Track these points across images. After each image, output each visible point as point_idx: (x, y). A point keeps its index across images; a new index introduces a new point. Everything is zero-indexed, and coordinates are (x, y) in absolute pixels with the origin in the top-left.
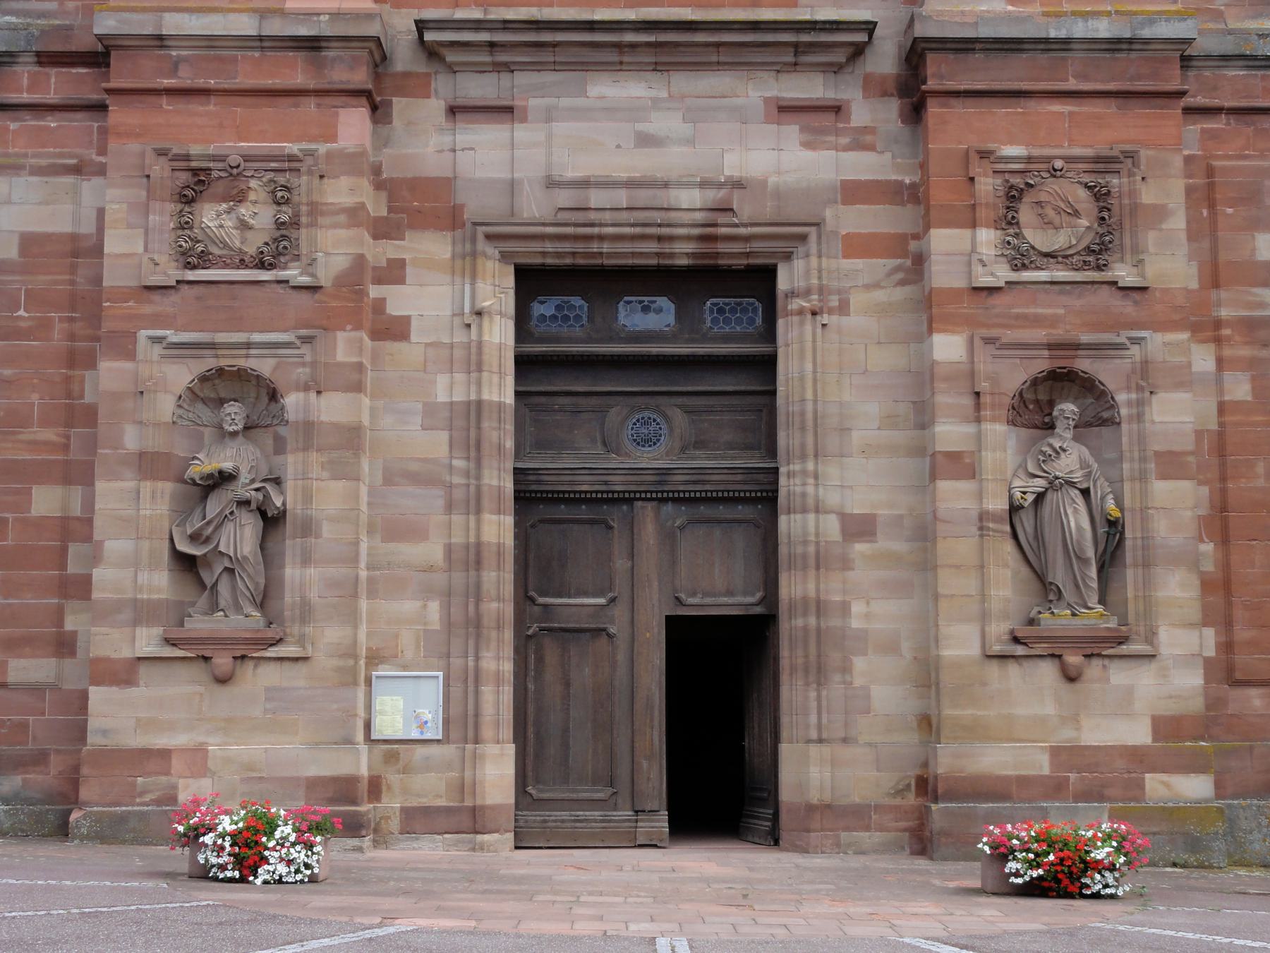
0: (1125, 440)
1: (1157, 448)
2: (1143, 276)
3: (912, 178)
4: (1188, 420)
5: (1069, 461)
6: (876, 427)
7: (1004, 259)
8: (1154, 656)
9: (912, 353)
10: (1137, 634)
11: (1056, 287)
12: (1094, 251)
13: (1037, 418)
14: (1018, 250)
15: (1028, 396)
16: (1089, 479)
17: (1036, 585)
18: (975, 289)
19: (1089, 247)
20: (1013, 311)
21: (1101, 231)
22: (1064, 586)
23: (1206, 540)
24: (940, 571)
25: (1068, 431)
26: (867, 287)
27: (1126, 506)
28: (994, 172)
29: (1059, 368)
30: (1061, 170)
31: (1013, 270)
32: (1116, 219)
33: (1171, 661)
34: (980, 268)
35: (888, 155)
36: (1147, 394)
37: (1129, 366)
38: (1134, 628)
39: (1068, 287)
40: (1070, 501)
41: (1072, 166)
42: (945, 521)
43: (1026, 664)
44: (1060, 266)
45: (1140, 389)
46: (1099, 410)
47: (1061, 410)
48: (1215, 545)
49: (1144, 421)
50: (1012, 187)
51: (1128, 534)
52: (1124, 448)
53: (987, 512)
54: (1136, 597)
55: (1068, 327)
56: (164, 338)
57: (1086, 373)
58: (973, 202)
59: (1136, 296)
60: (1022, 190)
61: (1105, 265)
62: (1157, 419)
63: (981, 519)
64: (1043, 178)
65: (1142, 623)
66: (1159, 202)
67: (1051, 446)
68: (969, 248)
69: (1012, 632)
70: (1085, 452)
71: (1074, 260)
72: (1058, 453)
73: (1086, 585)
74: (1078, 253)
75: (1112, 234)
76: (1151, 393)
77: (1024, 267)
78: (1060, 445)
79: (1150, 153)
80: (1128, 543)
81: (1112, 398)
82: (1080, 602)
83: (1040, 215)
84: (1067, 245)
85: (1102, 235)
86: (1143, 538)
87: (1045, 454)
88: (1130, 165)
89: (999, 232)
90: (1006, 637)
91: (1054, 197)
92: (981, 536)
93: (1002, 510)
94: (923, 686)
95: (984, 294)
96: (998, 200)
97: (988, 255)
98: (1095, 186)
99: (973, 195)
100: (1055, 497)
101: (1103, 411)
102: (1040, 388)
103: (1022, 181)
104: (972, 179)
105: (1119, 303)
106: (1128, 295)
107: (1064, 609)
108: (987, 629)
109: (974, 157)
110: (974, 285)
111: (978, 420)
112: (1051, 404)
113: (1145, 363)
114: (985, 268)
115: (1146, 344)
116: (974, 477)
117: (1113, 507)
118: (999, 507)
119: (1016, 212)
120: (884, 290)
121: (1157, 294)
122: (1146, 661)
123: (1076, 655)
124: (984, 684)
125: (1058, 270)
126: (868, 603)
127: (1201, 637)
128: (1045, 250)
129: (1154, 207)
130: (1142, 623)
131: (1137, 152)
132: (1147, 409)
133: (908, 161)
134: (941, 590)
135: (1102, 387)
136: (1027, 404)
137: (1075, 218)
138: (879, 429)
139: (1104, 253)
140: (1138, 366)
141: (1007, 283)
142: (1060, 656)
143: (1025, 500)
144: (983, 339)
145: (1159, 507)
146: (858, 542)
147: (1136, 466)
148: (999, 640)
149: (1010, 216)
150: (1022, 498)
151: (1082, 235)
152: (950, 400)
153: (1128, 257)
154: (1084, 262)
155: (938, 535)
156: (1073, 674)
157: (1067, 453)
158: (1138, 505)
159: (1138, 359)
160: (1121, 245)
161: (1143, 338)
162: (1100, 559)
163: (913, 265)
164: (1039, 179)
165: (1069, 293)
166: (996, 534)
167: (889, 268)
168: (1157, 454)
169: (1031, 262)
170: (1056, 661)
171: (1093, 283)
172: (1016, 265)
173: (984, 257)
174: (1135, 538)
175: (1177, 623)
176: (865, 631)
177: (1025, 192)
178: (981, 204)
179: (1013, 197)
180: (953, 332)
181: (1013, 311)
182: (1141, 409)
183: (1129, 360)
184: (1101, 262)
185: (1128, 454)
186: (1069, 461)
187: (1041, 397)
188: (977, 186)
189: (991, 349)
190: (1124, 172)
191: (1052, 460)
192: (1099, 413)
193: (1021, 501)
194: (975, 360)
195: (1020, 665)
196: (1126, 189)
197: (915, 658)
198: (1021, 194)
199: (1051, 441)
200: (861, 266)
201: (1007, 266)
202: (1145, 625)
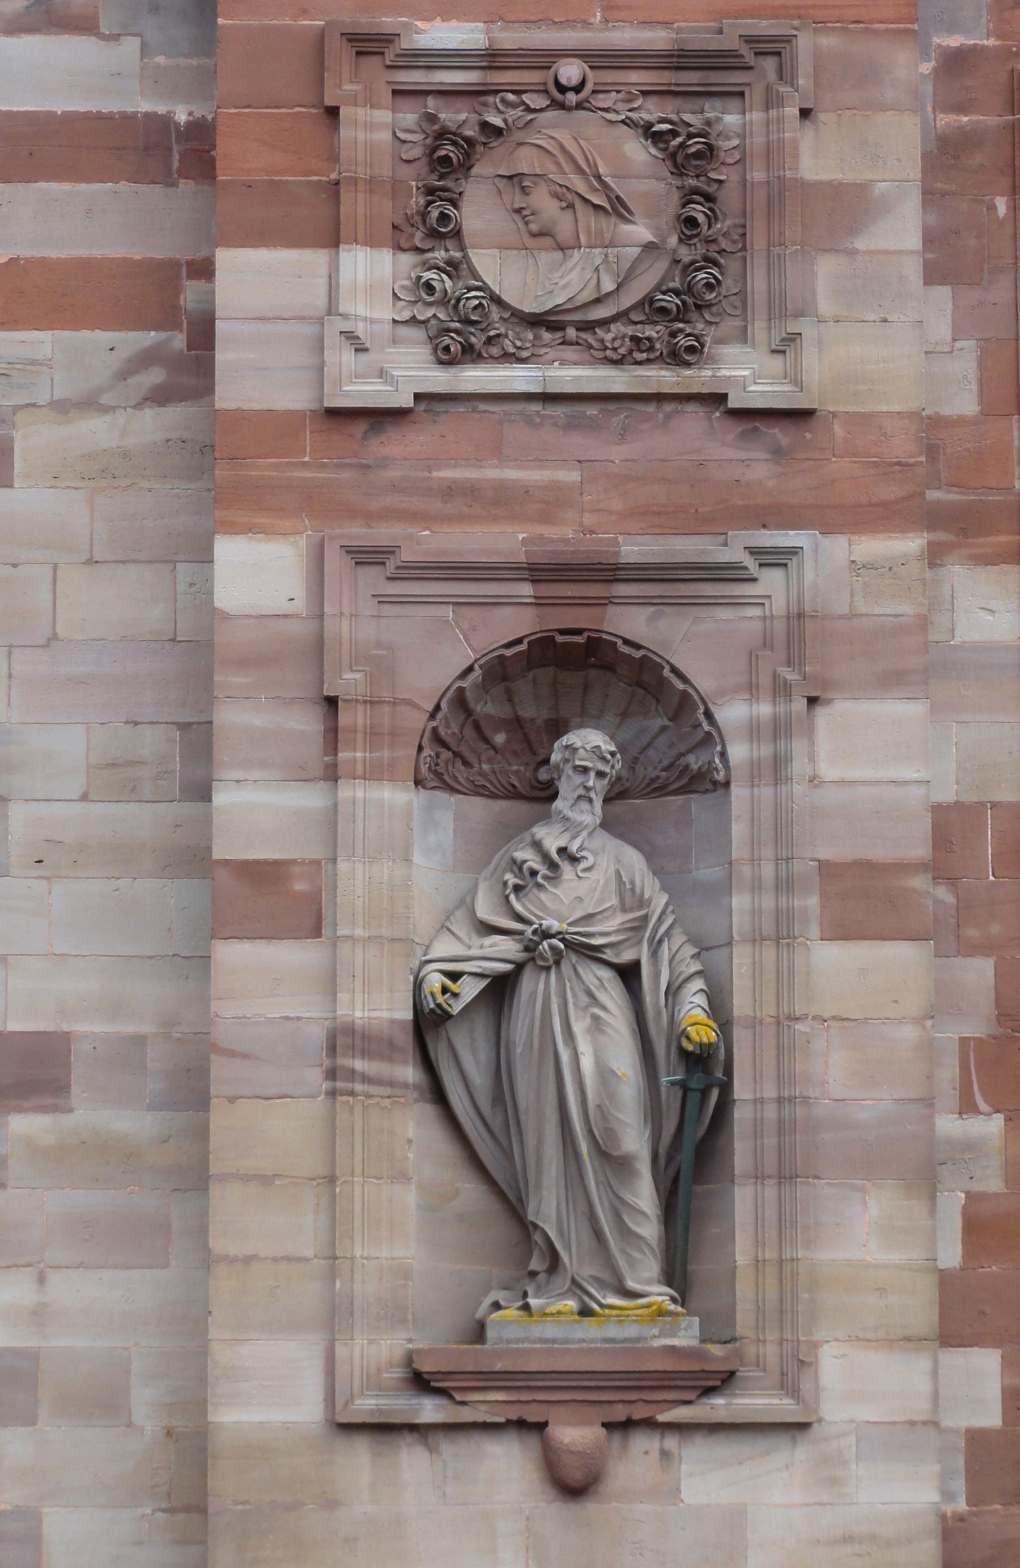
0: (738, 830)
1: (827, 853)
2: (798, 383)
3: (192, 107)
4: (916, 776)
5: (582, 889)
6: (75, 796)
7: (418, 334)
8: (803, 1427)
9: (181, 588)
10: (759, 1363)
11: (559, 411)
12: (664, 311)
13: (517, 771)
14: (456, 307)
15: (485, 708)
16: (640, 942)
17: (502, 1230)
18: (337, 415)
19: (652, 301)
20: (435, 474)
21: (685, 254)
22: (560, 1232)
23: (983, 1106)
24: (215, 1190)
25: (584, 805)
26: (62, 407)
27: (736, 1012)
28: (395, 92)
29: (563, 632)
30: (578, 89)
31: (441, 362)
32: (728, 222)
33: (852, 1439)
34: (348, 356)
35: (131, 46)
36: (799, 705)
37: (758, 625)
38: (751, 1351)
39: (592, 410)
40: (584, 999)
41: (610, 76)
42: (231, 1053)
43: (449, 1448)
44: (570, 353)
45: (781, 690)
46: (683, 747)
47: (567, 747)
48: (1008, 1119)
49: (789, 780)
50: (443, 134)
51: (741, 1090)
52: (735, 855)
53: (350, 1030)
54: (758, 1264)
55: (589, 520)
56: (390, 551)
57: (637, 646)
58: (333, 176)
59: (778, 434)
60: (469, 141)
61: (691, 350)
62: (828, 771)
63: (332, 1049)
64: (529, 110)
65: (772, 1336)
66: (849, 177)
67: (537, 845)
68: (322, 302)
69: (409, 1359)
70: (634, 860)
71: (609, 337)
72: (553, 866)
73: (625, 1232)
74: (621, 316)
75: (715, 263)
76: (812, 701)
77: (470, 354)
78: (562, 843)
79: (828, 42)
80: (741, 1115)
81: (708, 715)
82: (606, 1276)
83: (518, 211)
84: (588, 295)
85: (690, 268)
86: (780, 1100)
87: (520, 869)
88: (772, 76)
89: (407, 259)
90: (398, 1373)
91: (558, 164)
92: (333, 1094)
93: (393, 1021)
94: (189, 1509)
95: (360, 427)
96: (406, 172)
97: (372, 321)
98: (674, 133)
99: (333, 157)
100: (541, 986)
101: (690, 751)
102: (522, 687)
103: (474, 117)
104: (333, 112)
105: (731, 454)
106: (756, 429)
107: (562, 1296)
108: (341, 1351)
109: (340, 54)
110: (327, 404)
111: (332, 775)
112: (558, 728)
113: (798, 617)
114: (363, 357)
115: (800, 566)
116: (317, 932)
117: (700, 1015)
118: (385, 1014)
119: (455, 204)
120: (108, 418)
121: (838, 429)
122: (781, 1441)
123: (587, 1423)
124: (332, 1504)
125: (563, 362)
126: (41, 1280)
127: (935, 1374)
128: (529, 307)
129: (836, 191)
130: (772, 1336)
131: (788, 39)
132: (798, 746)
133: (182, 61)
134: (218, 1244)
135: (681, 686)
136: (488, 732)
137: (613, 219)
138: (84, 798)
139: (694, 315)
140: (779, 627)
141: (418, 397)
142: (541, 1427)
143: (455, 995)
144: (350, 551)
145: (827, 1015)
146: (20, 1110)
147: (768, 902)
148: (373, 1384)
149: (435, 214)
150: (445, 990)
151: (632, 269)
152: (259, 721)
153: (758, 328)
154: (635, 339)
155: (213, 1090)
156: (575, 1475)
157: (583, 865)
158: (769, 1010)
159: (778, 606)
160: (742, 294)
161: (794, 551)
162: (670, 1158)
163: (190, 348)
164: (518, 112)
165: (593, 426)
166: (374, 1090)
167: (124, 353)
168: (827, 869)
169: (490, 341)
170: (533, 1441)
171: (659, 398)
172: (447, 349)
173: (361, 325)
174: (759, 1102)
175: (870, 1335)
176: (33, 1356)
177: (480, 148)
178: (355, 181)
179: (446, 160)
180: (269, 532)
181: (435, 474)
182: (782, 744)
183: (756, 612)
184: (683, 341)
185: (746, 870)
186: (582, 889)
187: (528, 711)
188: (345, 132)
189: (372, 579)
190: (755, 95)
191: (539, 886)
192: (682, 755)
193: (440, 999)
194: (327, 609)
195: (432, 1450)
196: (757, 141)
197: (169, 1433)
198: (468, 155)
199: (540, 832)
200: (46, 351)
201: (424, 352)
202: (781, 1342)
